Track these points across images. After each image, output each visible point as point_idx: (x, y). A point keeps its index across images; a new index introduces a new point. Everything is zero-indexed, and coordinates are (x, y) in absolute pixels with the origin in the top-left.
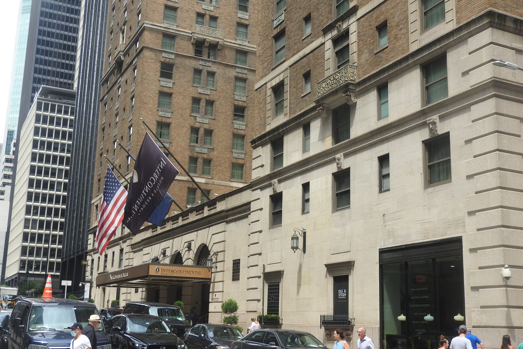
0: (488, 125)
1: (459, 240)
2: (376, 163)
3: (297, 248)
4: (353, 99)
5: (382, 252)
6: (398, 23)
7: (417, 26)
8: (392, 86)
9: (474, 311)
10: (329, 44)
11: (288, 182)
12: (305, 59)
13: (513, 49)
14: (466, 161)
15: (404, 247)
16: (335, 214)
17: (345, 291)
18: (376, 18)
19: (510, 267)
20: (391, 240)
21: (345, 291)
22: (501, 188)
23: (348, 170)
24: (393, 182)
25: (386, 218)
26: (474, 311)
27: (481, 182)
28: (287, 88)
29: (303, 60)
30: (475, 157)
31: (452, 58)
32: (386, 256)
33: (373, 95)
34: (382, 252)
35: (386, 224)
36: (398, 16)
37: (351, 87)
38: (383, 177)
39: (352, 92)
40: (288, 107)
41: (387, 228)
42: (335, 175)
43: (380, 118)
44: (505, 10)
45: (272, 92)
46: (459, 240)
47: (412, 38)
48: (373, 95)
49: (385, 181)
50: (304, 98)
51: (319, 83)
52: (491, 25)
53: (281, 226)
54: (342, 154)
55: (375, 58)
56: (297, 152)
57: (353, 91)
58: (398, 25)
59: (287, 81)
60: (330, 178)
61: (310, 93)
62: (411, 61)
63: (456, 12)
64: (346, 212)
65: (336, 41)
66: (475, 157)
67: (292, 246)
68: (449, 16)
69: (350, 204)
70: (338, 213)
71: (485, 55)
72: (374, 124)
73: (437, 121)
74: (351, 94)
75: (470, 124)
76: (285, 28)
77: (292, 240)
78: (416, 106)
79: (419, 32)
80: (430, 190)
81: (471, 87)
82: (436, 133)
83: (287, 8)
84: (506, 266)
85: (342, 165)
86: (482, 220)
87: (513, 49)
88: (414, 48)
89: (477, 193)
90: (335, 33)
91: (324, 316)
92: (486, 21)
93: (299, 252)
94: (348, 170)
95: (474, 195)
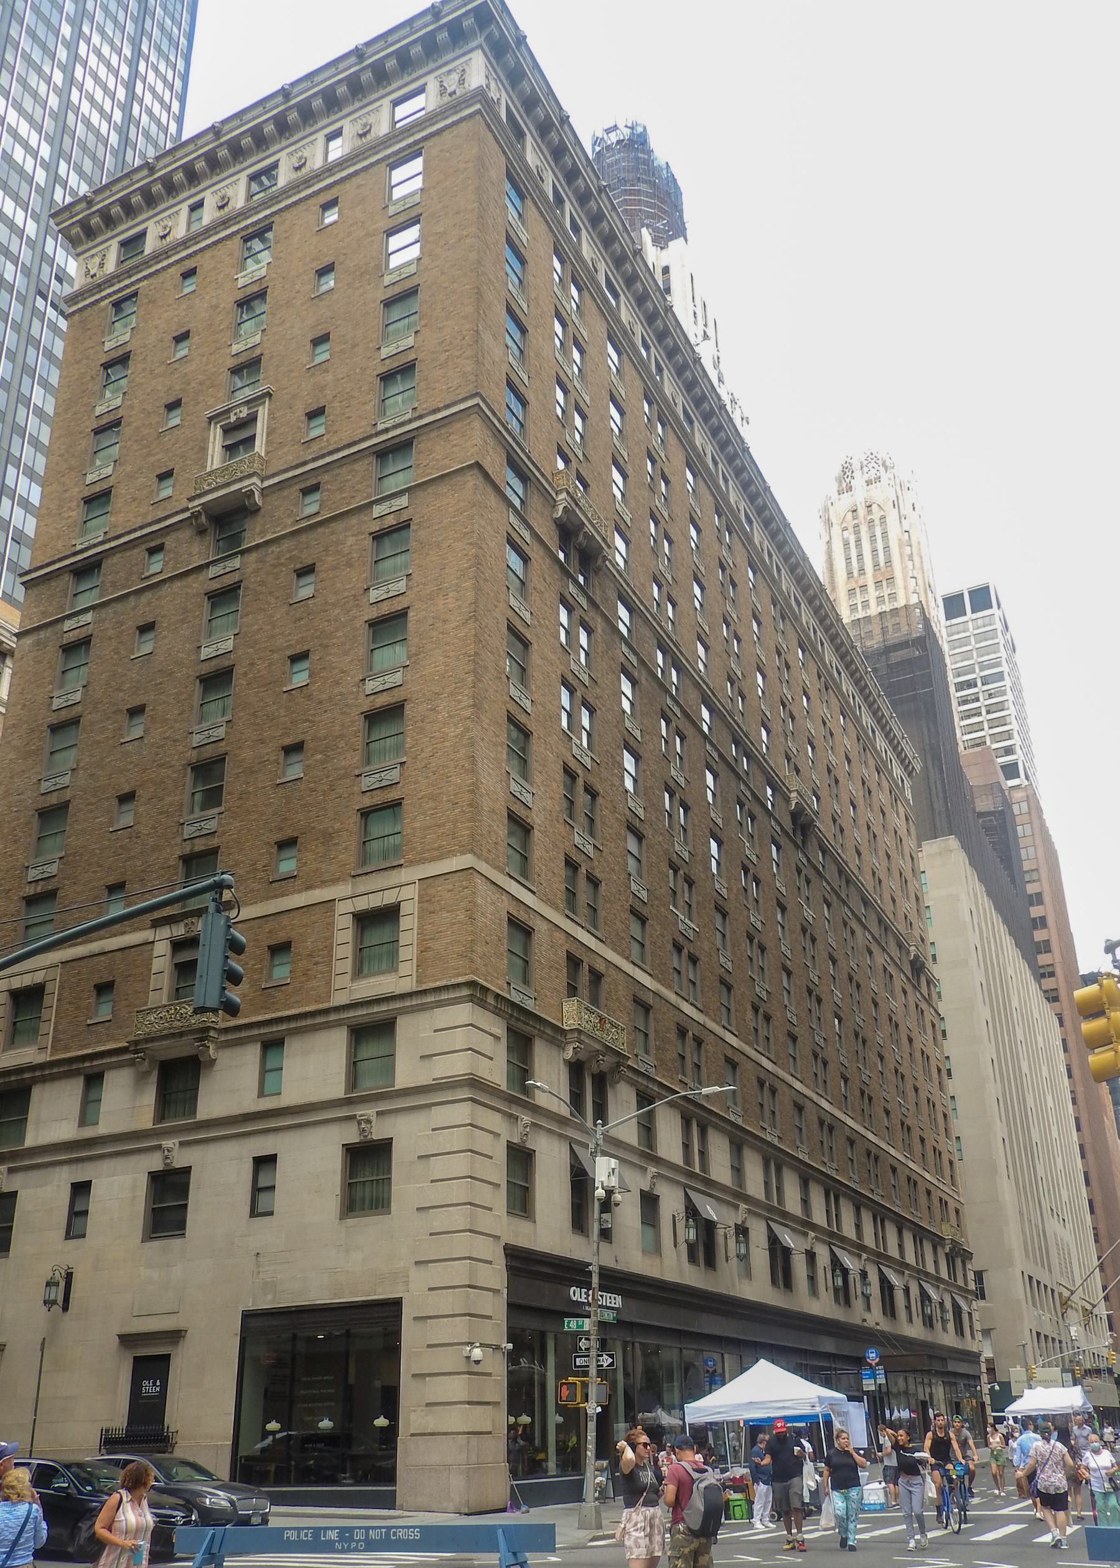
0: (456, 1139)
1: (397, 1303)
2: (248, 1167)
3: (54, 1302)
4: (211, 1051)
5: (247, 1316)
6: (313, 952)
7: (348, 966)
8: (292, 1046)
9: (414, 1411)
10: (162, 948)
11: (34, 1175)
12: (102, 958)
13: (491, 1035)
14: (418, 1186)
15: (293, 1309)
16: (148, 1244)
17: (158, 1384)
18: (270, 932)
19: (482, 1345)
20: (269, 1297)
21: (158, 1384)
22: (470, 1231)
23: (187, 1171)
24: (280, 1200)
25: (261, 1259)
26: (414, 1411)
27: (441, 1220)
28: (51, 1000)
29: (96, 959)
30: (432, 1181)
31: (404, 1027)
32: (254, 1323)
33: (251, 1055)
34: (247, 1316)
35: (261, 1269)
36: (312, 942)
37: (212, 1033)
38: (258, 1191)
39: (213, 1042)
40: (51, 1035)
41: (261, 1276)
42: (155, 1177)
43: (261, 1094)
44: (486, 980)
45: (9, 998)
46: (397, 1303)
47: (338, 982)
48: (251, 1055)
49: (263, 1197)
50: (94, 1028)
51: (141, 1011)
52: (471, 999)
53: (8, 1257)
54: (176, 1141)
55: (261, 995)
56: (64, 1123)
57: (214, 1040)
58: (311, 956)
59: (53, 988)
60: (143, 1181)
61: (110, 1021)
62: (333, 1017)
63: (418, 966)
64: (176, 1243)
65: (178, 945)
66: (432, 1181)
67: (47, 1298)
68: (405, 968)
69: (184, 1228)
70: (156, 1244)
71: (459, 1039)
72: (250, 1103)
73: (374, 1119)
74: (210, 1044)
75: (428, 1133)
76: (58, 889)
77: (48, 1288)
78: (336, 1089)
79: (348, 977)
80: (350, 1222)
81: (434, 1080)
82: (369, 1137)
83: (67, 855)
84: (478, 1345)
85: (175, 1161)
86: (438, 1275)
87: (491, 1035)
88: (340, 999)
89: (431, 1234)
90: (179, 931)
91: (107, 1431)
92: (465, 992)
93: (58, 1309)
94: (187, 1171)
95: (428, 1237)
